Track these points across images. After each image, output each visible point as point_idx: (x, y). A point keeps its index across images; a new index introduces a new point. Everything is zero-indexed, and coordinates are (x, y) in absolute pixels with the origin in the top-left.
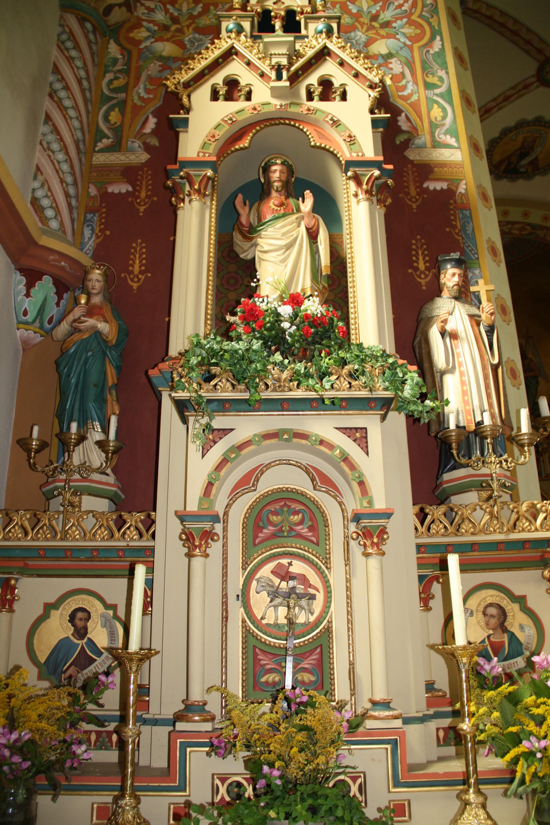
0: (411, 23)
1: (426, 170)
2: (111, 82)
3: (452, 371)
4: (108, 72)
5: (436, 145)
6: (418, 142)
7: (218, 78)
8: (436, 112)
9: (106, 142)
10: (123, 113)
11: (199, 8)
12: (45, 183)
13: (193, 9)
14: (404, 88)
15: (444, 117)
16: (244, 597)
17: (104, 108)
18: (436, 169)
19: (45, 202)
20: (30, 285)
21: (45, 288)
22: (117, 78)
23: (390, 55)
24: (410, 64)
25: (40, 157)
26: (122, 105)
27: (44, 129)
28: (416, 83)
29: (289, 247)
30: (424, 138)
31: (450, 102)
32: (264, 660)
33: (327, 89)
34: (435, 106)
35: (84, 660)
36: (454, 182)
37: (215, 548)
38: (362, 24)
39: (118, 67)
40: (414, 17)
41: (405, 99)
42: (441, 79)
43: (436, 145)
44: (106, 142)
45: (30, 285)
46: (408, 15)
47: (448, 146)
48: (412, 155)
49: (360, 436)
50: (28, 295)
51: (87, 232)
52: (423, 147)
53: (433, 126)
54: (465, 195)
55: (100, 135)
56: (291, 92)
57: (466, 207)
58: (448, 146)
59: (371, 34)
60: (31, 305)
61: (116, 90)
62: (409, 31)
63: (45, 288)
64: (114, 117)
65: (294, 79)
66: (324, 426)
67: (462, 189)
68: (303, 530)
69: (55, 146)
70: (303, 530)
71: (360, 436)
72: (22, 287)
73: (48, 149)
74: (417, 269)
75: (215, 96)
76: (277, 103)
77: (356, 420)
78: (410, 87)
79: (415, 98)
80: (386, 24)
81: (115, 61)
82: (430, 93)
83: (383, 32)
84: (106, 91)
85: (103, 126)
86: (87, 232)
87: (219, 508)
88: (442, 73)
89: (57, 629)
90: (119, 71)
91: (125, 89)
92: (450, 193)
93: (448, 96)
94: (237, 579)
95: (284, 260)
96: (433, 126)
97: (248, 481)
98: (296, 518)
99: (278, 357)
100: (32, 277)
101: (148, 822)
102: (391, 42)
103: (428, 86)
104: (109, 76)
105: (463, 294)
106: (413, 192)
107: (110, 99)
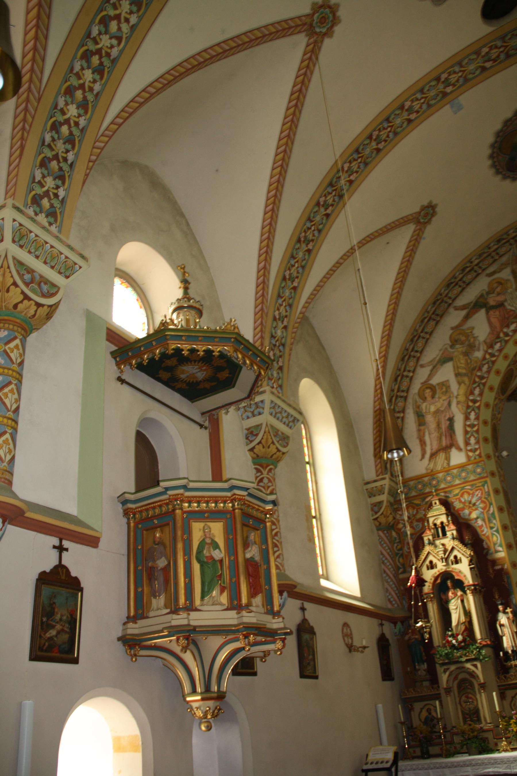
0: (483, 502)
1: (494, 562)
2: (396, 547)
3: (504, 636)
4: (394, 543)
5: (497, 551)
6: (490, 552)
7: (427, 562)
8: (495, 538)
9: (401, 570)
10: (403, 558)
11: (415, 512)
12: (390, 594)
13: (413, 512)
14: (483, 531)
15: (497, 540)
16: (460, 703)
17: (397, 558)
18: (498, 561)
19: (392, 600)
20: (395, 626)
21: (399, 625)
22: (398, 545)
23: (477, 518)
24: (484, 520)
25: (386, 585)
26: (402, 555)
27: (384, 575)
28: (487, 528)
29: (457, 608)
30: (492, 550)
31: (498, 532)
32: (466, 716)
33: (457, 561)
34: (494, 536)
35: (432, 720)
36: (503, 565)
37: (452, 694)
38: (467, 506)
39: (397, 541)
40: (483, 499)
41: (484, 535)
42: (495, 524)
43: (497, 551)
44: (401, 570)
45: (395, 626)
46: (480, 498)
47: (500, 551)
48: (489, 557)
49: (475, 666)
50: (395, 628)
51: (404, 602)
52: (492, 554)
53: (495, 544)
54: (507, 569)
55: (399, 568)
56: (447, 564)
57: (507, 573)
58: (500, 551)
59: (470, 510)
60: (397, 631)
61: (399, 550)
62: (482, 505)
63: (399, 625)
64: (401, 560)
65: (447, 559)
66: (468, 665)
67: (506, 567)
68: (469, 687)
69: (389, 580)
70: (469, 687)
71: (475, 666)
72: (393, 627)
73: (387, 582)
74: (495, 599)
75: (428, 569)
76: (444, 568)
77: (475, 663)
78: (485, 530)
79: (487, 534)
80: (474, 504)
81: (395, 538)
82: (492, 531)
83: (474, 508)
84: (396, 551)
85: (398, 564)
86: (404, 602)
87: (451, 685)
88: (494, 521)
89: (424, 714)
90: (398, 542)
91: (401, 549)
92: (502, 569)
93: (497, 531)
94: (458, 699)
95: (456, 613)
96: (495, 544)
97: (456, 678)
98: (467, 684)
99: (455, 651)
100: (395, 623)
101: (112, 357)
102: (477, 512)
103: (491, 528)
104: (396, 545)
105: (504, 612)
106: (491, 571)
107: (398, 554)
